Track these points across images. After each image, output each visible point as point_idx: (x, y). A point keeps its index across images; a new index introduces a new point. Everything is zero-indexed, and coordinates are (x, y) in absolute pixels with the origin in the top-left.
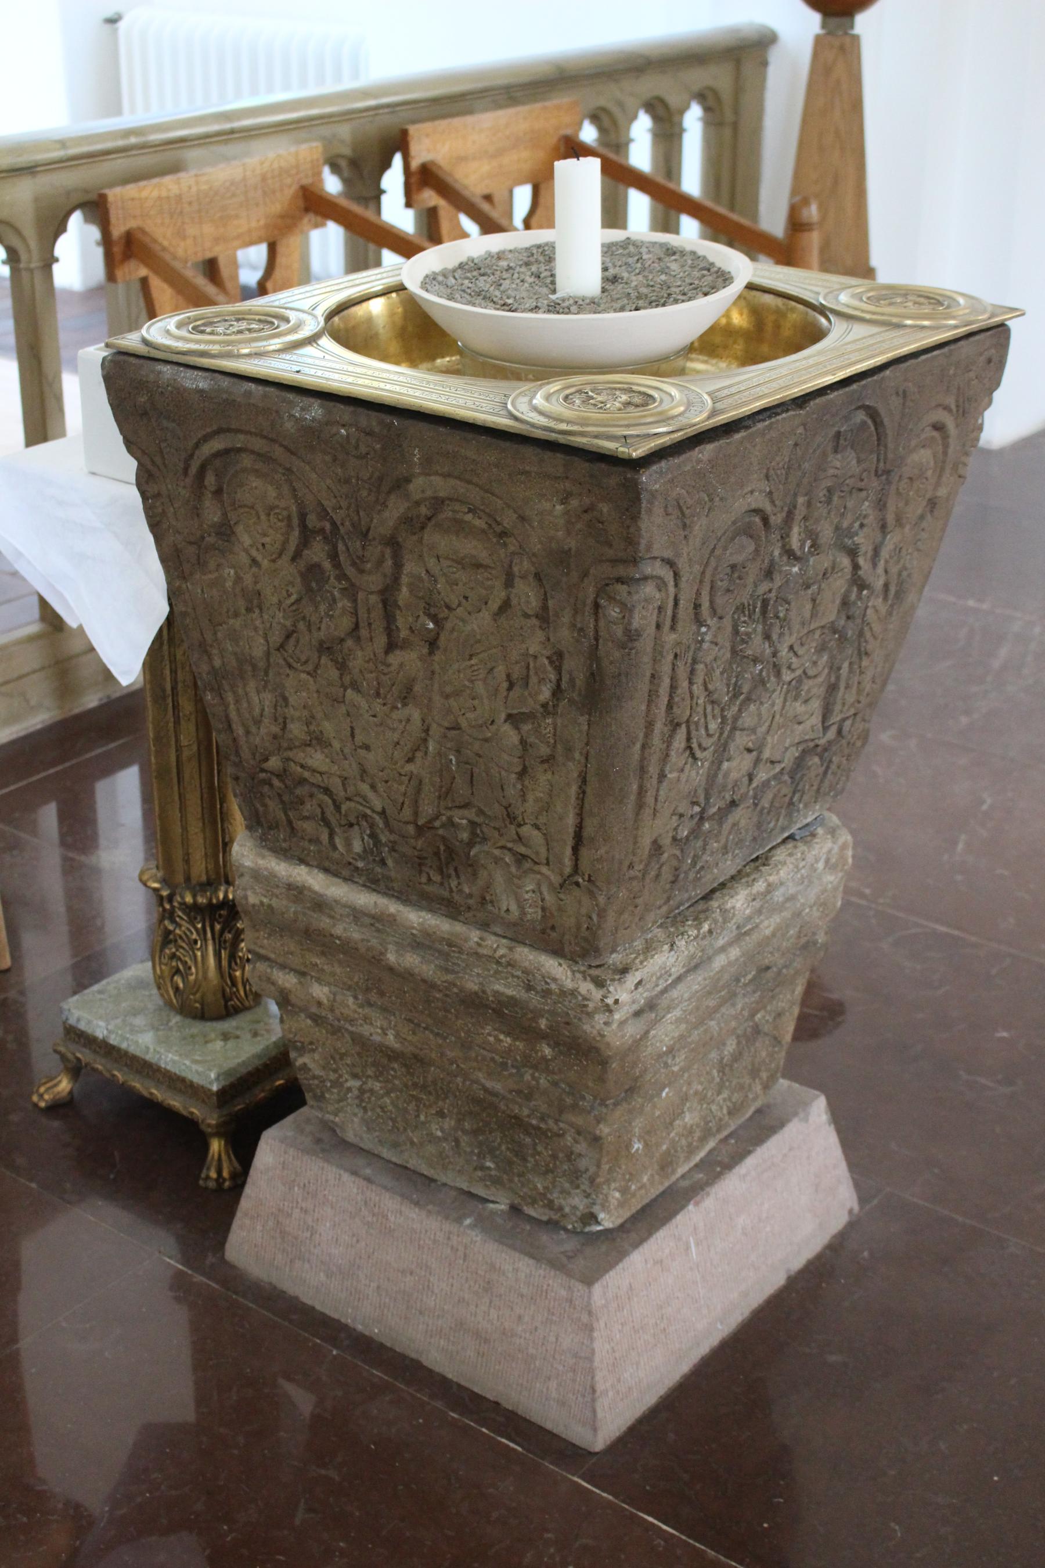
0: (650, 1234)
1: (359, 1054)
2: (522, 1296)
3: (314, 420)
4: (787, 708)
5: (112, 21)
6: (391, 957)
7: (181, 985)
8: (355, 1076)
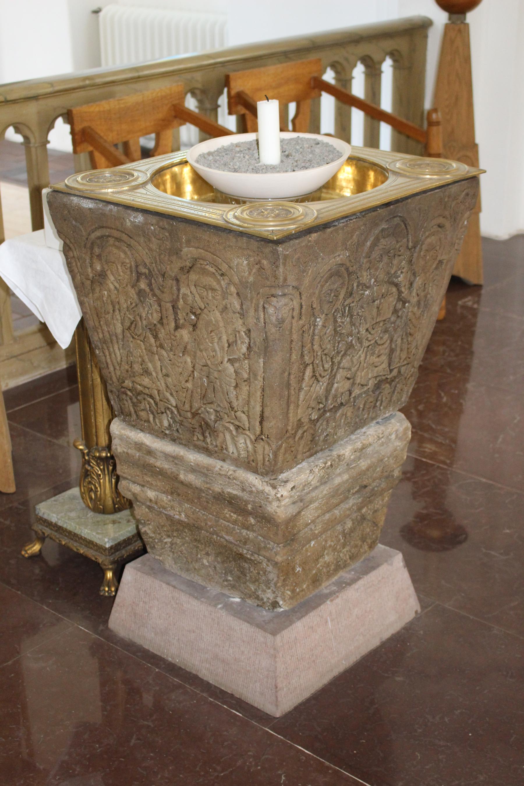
0: (307, 613)
1: (170, 525)
2: (244, 641)
3: (139, 222)
4: (368, 359)
5: (97, 12)
6: (182, 477)
7: (93, 497)
8: (169, 536)
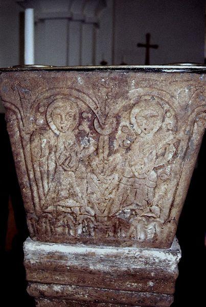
6: (92, 267)
